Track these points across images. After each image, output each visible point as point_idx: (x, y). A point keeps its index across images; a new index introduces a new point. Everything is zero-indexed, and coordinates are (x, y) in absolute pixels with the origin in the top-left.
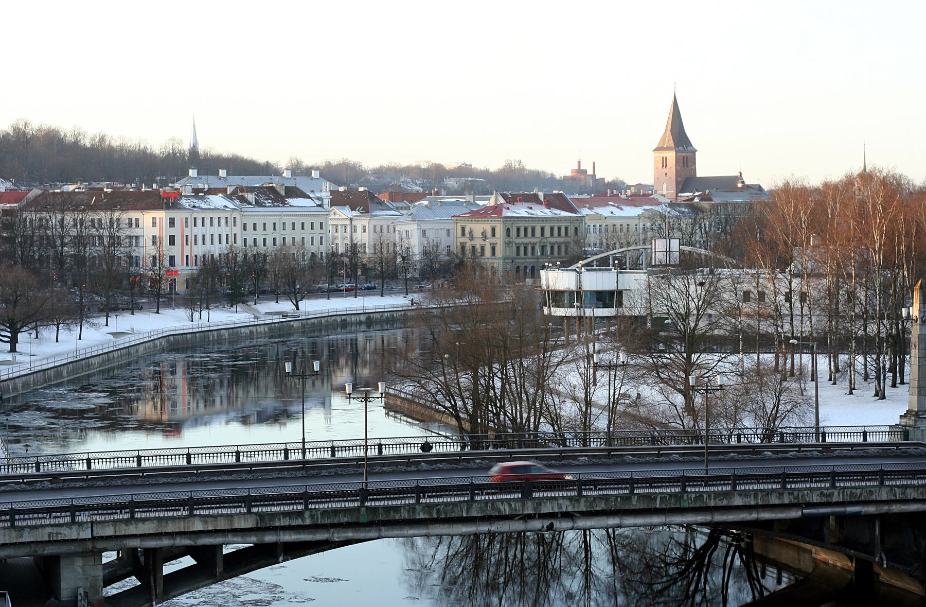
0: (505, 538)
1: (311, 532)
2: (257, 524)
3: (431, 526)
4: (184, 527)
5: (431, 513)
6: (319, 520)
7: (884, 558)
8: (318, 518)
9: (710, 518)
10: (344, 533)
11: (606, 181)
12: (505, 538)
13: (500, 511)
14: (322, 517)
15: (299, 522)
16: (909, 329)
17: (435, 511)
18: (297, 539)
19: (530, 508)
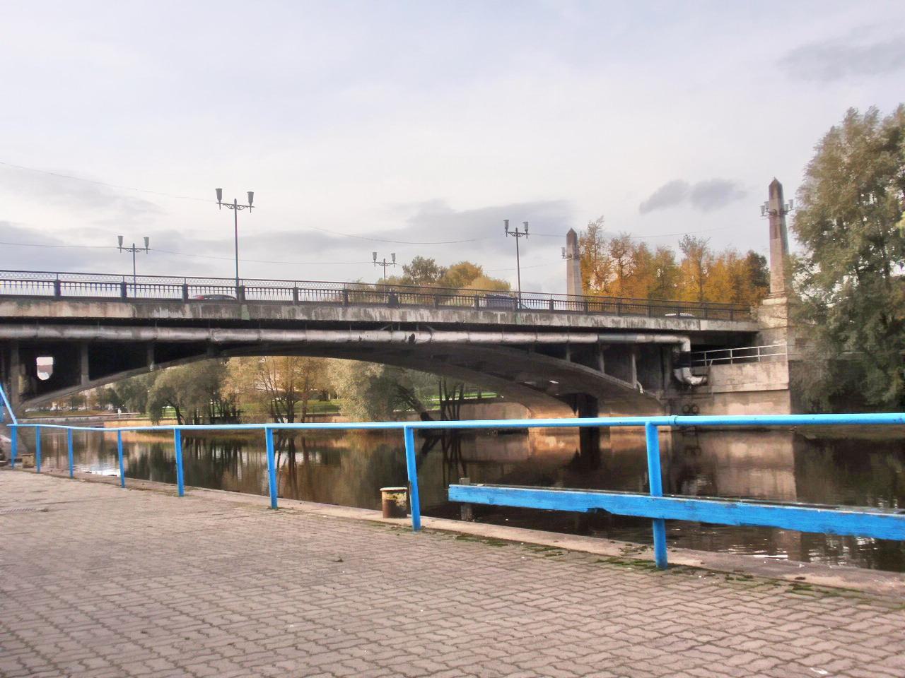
0: (204, 537)
1: (190, 330)
2: (134, 314)
3: (307, 331)
4: (50, 312)
5: (309, 315)
6: (201, 315)
7: (641, 386)
8: (199, 313)
9: (482, 394)
10: (224, 332)
11: (167, 310)
12: (204, 537)
13: (371, 317)
14: (204, 312)
15: (177, 315)
16: (611, 245)
17: (313, 314)
18: (176, 336)
19: (397, 316)
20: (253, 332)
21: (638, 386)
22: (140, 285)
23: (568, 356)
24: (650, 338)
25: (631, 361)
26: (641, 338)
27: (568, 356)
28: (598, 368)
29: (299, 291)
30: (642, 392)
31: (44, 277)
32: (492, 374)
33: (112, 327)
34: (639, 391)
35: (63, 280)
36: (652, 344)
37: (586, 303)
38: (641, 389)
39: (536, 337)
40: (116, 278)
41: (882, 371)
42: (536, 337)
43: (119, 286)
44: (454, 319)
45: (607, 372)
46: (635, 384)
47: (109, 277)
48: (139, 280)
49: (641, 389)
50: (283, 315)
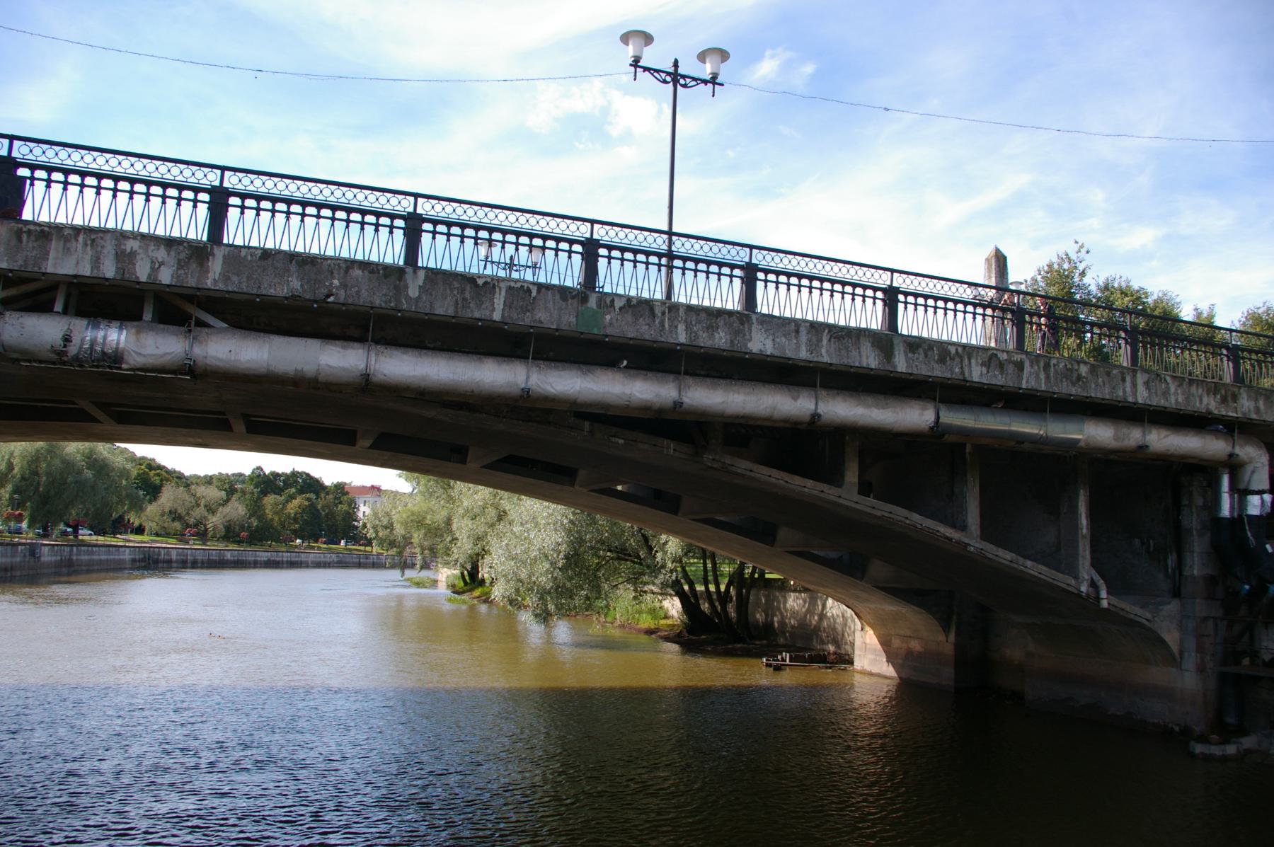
7: (1101, 583)
20: (410, 354)
21: (1093, 584)
22: (685, 259)
23: (852, 475)
24: (1133, 436)
25: (1074, 510)
26: (1099, 434)
27: (852, 475)
28: (963, 528)
29: (761, 275)
30: (1105, 604)
31: (562, 228)
32: (705, 521)
33: (337, 342)
34: (1098, 599)
35: (903, 287)
36: (1141, 460)
37: (670, 256)
38: (1104, 594)
39: (1144, 435)
40: (573, 226)
41: (223, 534)
42: (1144, 435)
43: (879, 294)
44: (1175, 398)
45: (984, 537)
46: (1084, 578)
47: (632, 234)
48: (679, 246)
49: (1104, 594)
50: (864, 359)
